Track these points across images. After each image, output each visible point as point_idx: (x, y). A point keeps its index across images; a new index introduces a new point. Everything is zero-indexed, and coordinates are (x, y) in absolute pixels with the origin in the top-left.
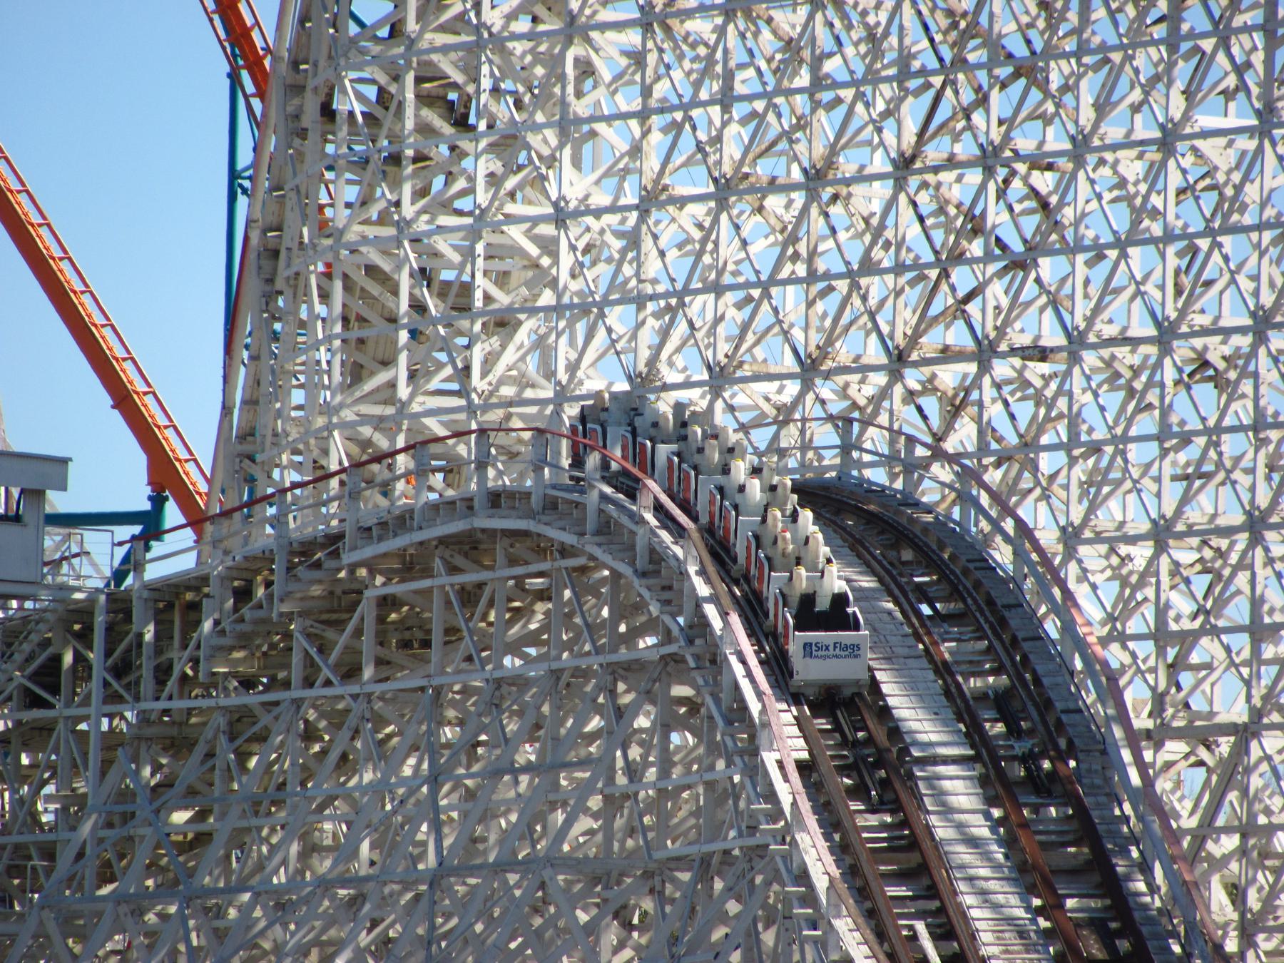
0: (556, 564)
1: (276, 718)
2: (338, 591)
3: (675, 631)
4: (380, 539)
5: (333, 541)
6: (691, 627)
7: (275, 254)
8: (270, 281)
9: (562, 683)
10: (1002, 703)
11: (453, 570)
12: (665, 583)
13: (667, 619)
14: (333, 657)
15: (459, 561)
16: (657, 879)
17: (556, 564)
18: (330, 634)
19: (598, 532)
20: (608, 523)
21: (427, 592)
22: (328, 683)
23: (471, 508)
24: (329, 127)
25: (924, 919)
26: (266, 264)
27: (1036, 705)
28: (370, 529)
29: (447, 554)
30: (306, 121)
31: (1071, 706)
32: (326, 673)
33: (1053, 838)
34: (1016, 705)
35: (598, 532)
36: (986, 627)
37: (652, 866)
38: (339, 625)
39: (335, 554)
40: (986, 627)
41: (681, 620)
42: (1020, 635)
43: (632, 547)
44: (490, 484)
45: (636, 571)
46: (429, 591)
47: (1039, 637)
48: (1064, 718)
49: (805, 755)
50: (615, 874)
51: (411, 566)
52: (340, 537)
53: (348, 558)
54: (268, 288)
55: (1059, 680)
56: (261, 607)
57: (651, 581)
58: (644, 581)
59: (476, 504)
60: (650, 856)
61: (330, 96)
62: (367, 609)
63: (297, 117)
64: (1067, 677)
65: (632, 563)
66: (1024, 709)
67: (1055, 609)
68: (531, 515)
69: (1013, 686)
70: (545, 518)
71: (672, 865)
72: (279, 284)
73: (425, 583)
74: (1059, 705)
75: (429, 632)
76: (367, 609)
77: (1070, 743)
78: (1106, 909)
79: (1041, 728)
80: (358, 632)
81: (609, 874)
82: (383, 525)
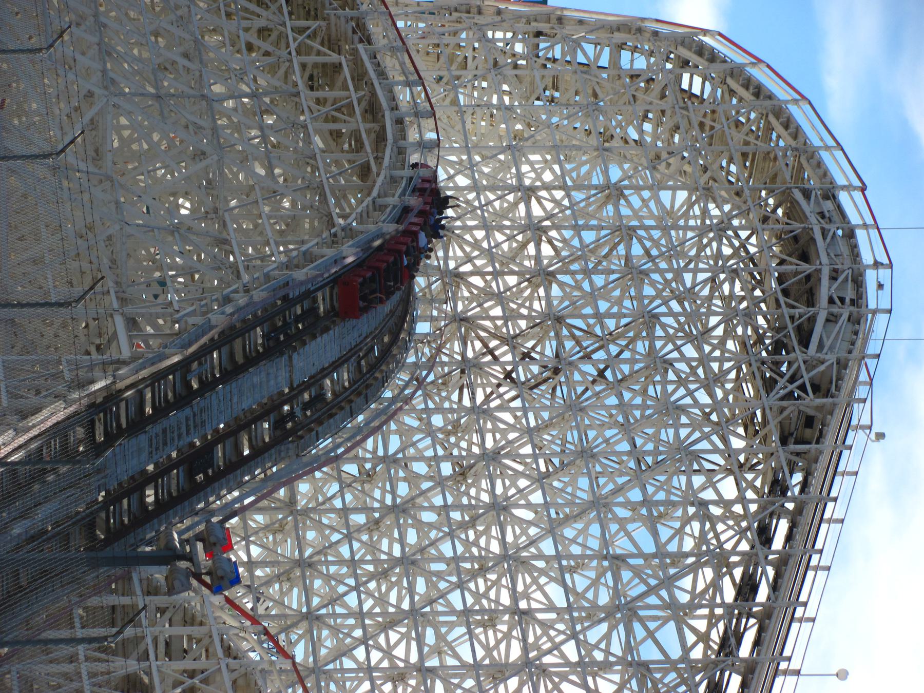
0: (370, 155)
1: (274, 13)
2: (340, 43)
3: (349, 221)
4: (372, 63)
5: (367, 39)
6: (351, 229)
7: (468, 12)
8: (456, 10)
9: (308, 160)
10: (319, 398)
11: (359, 100)
12: (370, 215)
13: (354, 216)
14: (309, 42)
15: (364, 104)
16: (214, 216)
17: (370, 155)
18: (319, 40)
19: (391, 177)
20: (396, 182)
21: (346, 88)
22: (295, 39)
23: (392, 109)
24: (531, 35)
25: (431, 556)
26: (464, 8)
27: (320, 417)
28: (375, 58)
29: (367, 98)
30: (534, 24)
31: (320, 436)
32: (300, 38)
33: (254, 433)
34: (319, 406)
35: (391, 177)
36: (356, 386)
37: (220, 212)
38: (322, 44)
39: (361, 41)
40: (356, 386)
41: (354, 224)
42: (353, 405)
43: (386, 196)
44: (407, 119)
45: (375, 198)
46: (348, 89)
47: (353, 415)
48: (314, 433)
49: (291, 296)
50: (215, 193)
51: (360, 76)
52: (370, 43)
53: (360, 47)
54: (452, 9)
55: (333, 427)
56: (330, 4)
57: (371, 208)
58: (371, 203)
59: (396, 112)
60: (226, 211)
61: (546, 35)
62: (334, 57)
63: (536, 20)
64: (334, 432)
65: (379, 196)
66: (317, 411)
67: (367, 423)
68: (395, 141)
69: (328, 404)
70: (395, 149)
71: (221, 223)
72: (455, 15)
73: (351, 88)
74: (320, 429)
75: (318, 90)
76: (334, 57)
77: (301, 437)
78: (219, 466)
79: (308, 421)
80: (319, 53)
81: (213, 188)
82: (379, 64)
